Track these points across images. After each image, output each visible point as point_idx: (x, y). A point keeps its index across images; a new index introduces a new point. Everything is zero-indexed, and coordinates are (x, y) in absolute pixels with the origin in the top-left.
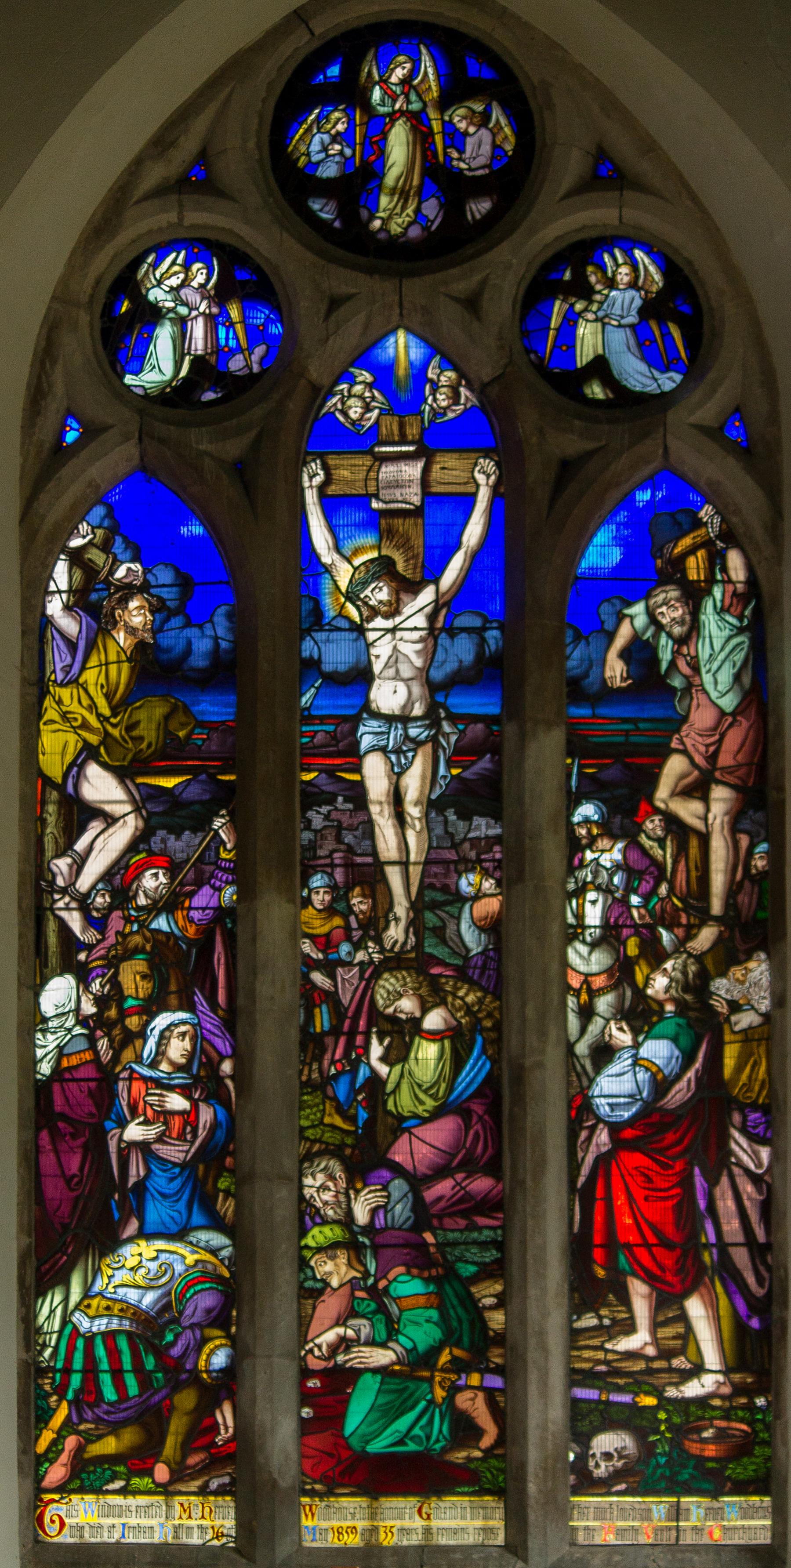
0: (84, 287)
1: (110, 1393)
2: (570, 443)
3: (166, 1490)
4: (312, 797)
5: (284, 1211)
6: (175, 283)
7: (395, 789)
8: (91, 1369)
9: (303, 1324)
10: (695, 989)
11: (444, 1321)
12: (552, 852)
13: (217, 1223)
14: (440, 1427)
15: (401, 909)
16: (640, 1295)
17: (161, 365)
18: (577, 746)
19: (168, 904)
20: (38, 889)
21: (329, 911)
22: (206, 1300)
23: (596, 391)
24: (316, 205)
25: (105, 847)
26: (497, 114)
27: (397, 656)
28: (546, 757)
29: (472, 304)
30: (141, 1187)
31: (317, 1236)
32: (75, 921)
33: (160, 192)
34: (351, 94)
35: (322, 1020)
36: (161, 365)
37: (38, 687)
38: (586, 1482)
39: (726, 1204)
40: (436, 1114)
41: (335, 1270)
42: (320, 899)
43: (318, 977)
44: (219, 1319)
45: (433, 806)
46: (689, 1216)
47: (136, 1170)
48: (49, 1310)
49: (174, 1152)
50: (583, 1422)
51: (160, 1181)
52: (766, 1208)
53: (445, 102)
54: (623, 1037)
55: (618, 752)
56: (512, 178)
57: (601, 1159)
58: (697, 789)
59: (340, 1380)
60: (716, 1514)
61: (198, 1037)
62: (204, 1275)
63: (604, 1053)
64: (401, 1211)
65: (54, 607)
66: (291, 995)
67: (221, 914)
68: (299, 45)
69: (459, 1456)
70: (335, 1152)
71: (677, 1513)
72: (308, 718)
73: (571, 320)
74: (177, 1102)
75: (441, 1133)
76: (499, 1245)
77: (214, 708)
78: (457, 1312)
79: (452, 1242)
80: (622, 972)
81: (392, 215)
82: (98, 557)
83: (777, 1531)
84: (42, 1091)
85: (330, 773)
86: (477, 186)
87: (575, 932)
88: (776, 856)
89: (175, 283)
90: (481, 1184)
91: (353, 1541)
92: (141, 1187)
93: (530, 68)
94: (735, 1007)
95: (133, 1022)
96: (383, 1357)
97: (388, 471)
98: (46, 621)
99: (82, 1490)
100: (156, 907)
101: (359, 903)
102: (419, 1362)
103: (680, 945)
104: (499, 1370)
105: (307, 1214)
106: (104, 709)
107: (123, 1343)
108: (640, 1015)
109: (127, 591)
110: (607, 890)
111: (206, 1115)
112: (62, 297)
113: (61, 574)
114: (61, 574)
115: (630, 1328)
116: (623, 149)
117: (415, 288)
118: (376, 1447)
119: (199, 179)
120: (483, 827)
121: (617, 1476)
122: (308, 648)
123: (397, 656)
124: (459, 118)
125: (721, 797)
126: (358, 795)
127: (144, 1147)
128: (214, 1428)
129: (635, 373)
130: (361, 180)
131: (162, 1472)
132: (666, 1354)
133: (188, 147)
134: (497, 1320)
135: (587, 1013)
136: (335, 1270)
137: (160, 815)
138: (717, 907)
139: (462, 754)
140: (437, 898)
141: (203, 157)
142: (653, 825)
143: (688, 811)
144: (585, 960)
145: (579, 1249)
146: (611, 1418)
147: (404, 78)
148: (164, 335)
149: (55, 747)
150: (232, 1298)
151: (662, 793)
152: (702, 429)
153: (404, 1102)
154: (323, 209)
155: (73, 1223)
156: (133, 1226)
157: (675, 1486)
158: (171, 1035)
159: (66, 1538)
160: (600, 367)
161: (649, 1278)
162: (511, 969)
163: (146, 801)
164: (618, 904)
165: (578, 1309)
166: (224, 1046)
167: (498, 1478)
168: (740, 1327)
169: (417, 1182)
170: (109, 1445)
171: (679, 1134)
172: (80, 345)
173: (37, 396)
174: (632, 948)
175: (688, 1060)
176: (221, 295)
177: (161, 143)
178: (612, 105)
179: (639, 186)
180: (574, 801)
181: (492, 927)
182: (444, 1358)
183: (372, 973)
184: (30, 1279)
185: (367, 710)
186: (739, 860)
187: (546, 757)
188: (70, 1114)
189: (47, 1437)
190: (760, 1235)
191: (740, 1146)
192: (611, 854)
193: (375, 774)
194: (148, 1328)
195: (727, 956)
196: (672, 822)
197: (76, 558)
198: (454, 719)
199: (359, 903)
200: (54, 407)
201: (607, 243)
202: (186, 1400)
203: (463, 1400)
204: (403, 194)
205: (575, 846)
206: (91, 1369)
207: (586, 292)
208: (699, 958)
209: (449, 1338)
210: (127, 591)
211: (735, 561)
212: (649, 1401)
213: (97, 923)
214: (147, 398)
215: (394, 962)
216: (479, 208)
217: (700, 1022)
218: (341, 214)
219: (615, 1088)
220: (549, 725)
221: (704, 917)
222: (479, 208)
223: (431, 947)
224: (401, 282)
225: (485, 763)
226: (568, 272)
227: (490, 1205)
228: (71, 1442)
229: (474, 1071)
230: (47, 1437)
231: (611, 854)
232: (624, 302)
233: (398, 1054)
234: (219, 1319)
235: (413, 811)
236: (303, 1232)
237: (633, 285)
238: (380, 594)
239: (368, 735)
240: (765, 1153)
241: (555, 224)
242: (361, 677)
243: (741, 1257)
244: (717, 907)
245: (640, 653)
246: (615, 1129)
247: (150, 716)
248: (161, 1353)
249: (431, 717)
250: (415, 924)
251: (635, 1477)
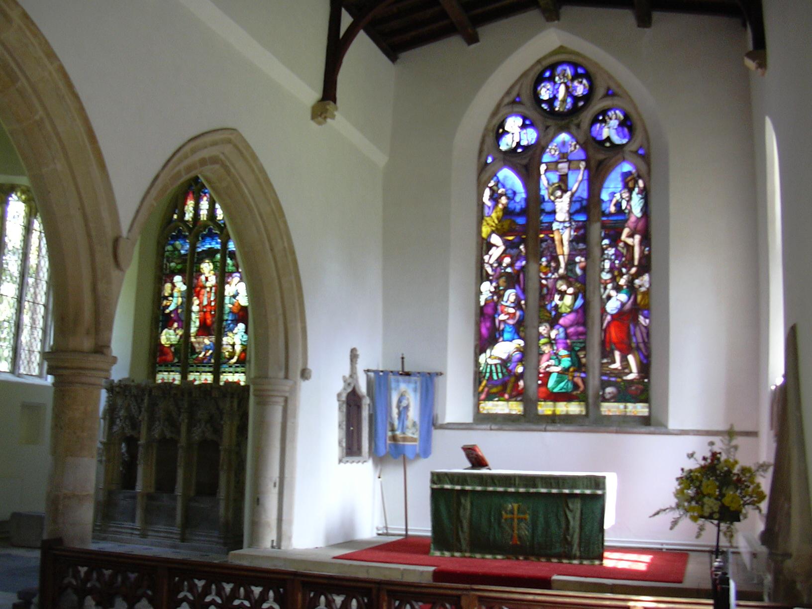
0: (491, 127)
1: (495, 377)
2: (601, 156)
3: (507, 400)
4: (543, 240)
5: (534, 335)
6: (513, 124)
8: (491, 372)
9: (539, 362)
10: (631, 283)
11: (572, 361)
13: (520, 338)
14: (570, 385)
15: (563, 265)
16: (617, 355)
18: (604, 226)
19: (511, 265)
20: (481, 263)
21: (547, 266)
22: (517, 355)
23: (519, 150)
24: (543, 106)
25: (495, 253)
28: (596, 230)
30: (503, 330)
31: (543, 341)
33: (508, 104)
35: (545, 291)
37: (481, 218)
38: (605, 400)
40: (570, 312)
41: (546, 349)
42: (544, 264)
43: (544, 282)
44: (521, 361)
45: (571, 242)
47: (502, 326)
48: (482, 359)
49: (511, 322)
50: (604, 385)
51: (508, 329)
56: (587, 98)
57: (609, 323)
58: (631, 236)
59: (548, 374)
60: (635, 407)
61: (517, 295)
62: (518, 349)
63: (609, 297)
64: (562, 335)
66: (537, 286)
67: (523, 268)
68: (539, 68)
69: (575, 393)
70: (547, 321)
71: (626, 407)
73: (601, 128)
74: (512, 311)
75: (571, 317)
76: (584, 342)
77: (521, 221)
78: (575, 359)
80: (614, 279)
82: (495, 188)
83: (650, 412)
84: (482, 308)
85: (547, 235)
87: (603, 270)
90: (581, 329)
91: (549, 413)
92: (503, 330)
94: (640, 286)
95: (502, 292)
98: (483, 203)
99: (489, 400)
100: (508, 266)
101: (553, 264)
102: (565, 371)
103: (627, 273)
104: (584, 372)
105: (540, 335)
106: (496, 221)
107: (499, 366)
108: (618, 289)
109: (501, 195)
110: (610, 260)
111: (518, 313)
112: (486, 129)
116: (614, 88)
118: (556, 390)
120: (581, 246)
121: (612, 398)
125: (637, 237)
127: (504, 321)
128: (518, 386)
129: (617, 140)
131: (506, 396)
132: (624, 368)
133: (514, 93)
134: (584, 360)
135: (605, 288)
136: (546, 349)
137: (509, 245)
138: (636, 263)
140: (571, 263)
141: (518, 96)
142: (621, 244)
143: (630, 241)
144: (606, 276)
145: (603, 344)
146: (610, 384)
149: (485, 230)
151: (623, 237)
152: (632, 152)
153: (563, 310)
155: (486, 339)
156: (501, 339)
158: (510, 295)
159: (485, 412)
161: (620, 350)
162: (587, 279)
163: (506, 242)
164: (613, 263)
165: (603, 357)
166: (522, 297)
169: (566, 328)
170: (494, 390)
172: (490, 140)
173: (481, 152)
174: (616, 273)
175: (629, 299)
177: (508, 93)
178: (611, 77)
182: (571, 369)
183: (556, 280)
184: (478, 351)
185: (555, 220)
186: (642, 252)
187: (596, 230)
189: (481, 388)
190: (646, 340)
192: (611, 251)
194: (504, 363)
195: (638, 275)
197: (491, 188)
198: (575, 221)
199: (553, 264)
200: (484, 154)
201: (609, 109)
202: (513, 379)
203: (576, 379)
206: (491, 372)
208: (632, 275)
209: (573, 365)
210: (501, 195)
212: (619, 380)
215: (561, 277)
217: (632, 289)
218: (549, 107)
219: (612, 307)
220: (596, 222)
221: (633, 266)
222: (581, 104)
223: (570, 274)
225: (582, 231)
227: (584, 334)
228: (486, 389)
229: (579, 302)
230: (481, 388)
231: (611, 251)
232: (614, 123)
233: (561, 299)
234: (521, 361)
236: (539, 340)
237: (616, 119)
240: (647, 321)
241: (597, 106)
242: (554, 212)
243: (641, 346)
244: (636, 263)
248: (507, 368)
250: (566, 269)
251: (616, 399)
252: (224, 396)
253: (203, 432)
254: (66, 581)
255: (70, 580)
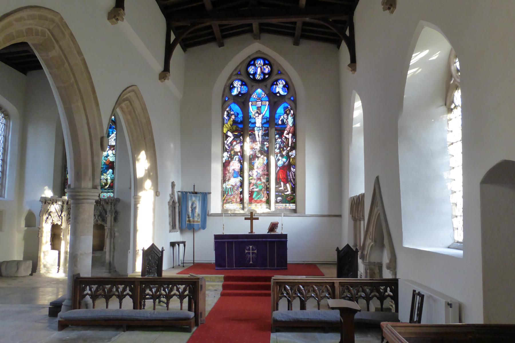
0: (228, 85)
2: (276, 100)
6: (237, 84)
10: (288, 154)
12: (274, 140)
16: (282, 183)
17: (235, 92)
18: (276, 130)
23: (278, 95)
25: (230, 140)
26: (269, 67)
27: (259, 122)
28: (273, 131)
29: (266, 86)
32: (227, 147)
34: (254, 65)
36: (235, 92)
37: (223, 124)
39: (291, 175)
46: (287, 176)
48: (224, 185)
52: (295, 175)
53: (263, 66)
54: (280, 158)
55: (280, 130)
56: (270, 74)
58: (288, 134)
65: (225, 116)
68: (249, 60)
71: (286, 205)
72: (250, 127)
77: (241, 126)
80: (280, 152)
81: (258, 77)
86: (267, 74)
87: (276, 148)
88: (296, 141)
89: (237, 84)
93: (272, 62)
96: (257, 190)
97: (258, 103)
103: (286, 149)
109: (232, 115)
113: (226, 113)
114: (226, 113)
115: (281, 187)
116: (281, 70)
117: (260, 84)
119: (239, 74)
120: (267, 138)
121: (280, 202)
122: (250, 120)
123: (259, 122)
124: (265, 67)
125: (290, 135)
126: (255, 135)
129: (282, 93)
130: (255, 74)
132: (285, 189)
133: (238, 70)
139: (265, 131)
141: (240, 71)
142: (284, 137)
143: (287, 136)
147: (260, 62)
148: (236, 89)
149: (225, 130)
151: (285, 134)
154: (251, 77)
157: (286, 203)
160: (279, 92)
163: (234, 135)
168: (292, 187)
172: (227, 90)
176: (241, 85)
177: (235, 70)
179: (283, 74)
180: (276, 135)
181: (268, 147)
186: (292, 141)
191: (292, 169)
193: (256, 133)
195: (291, 150)
196: (285, 137)
197: (227, 111)
200: (225, 96)
204: (259, 75)
205: (276, 140)
207: (277, 85)
210: (232, 115)
211: (292, 112)
213: (229, 147)
214: (234, 96)
216: (267, 76)
217: (288, 157)
221: (289, 146)
224: (252, 231)
226: (275, 83)
231: (279, 140)
232: (281, 86)
235: (260, 136)
238: (257, 115)
239: (256, 129)
242: (255, 123)
243: (292, 180)
245: (282, 121)
246: (280, 167)
247: (234, 127)
249: (262, 127)
252: (107, 203)
253: (97, 221)
254: (85, 292)
255: (88, 291)
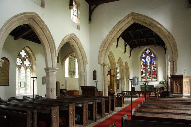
6: (143, 55)
7: (148, 65)
25: (142, 66)
79: (150, 74)
89: (143, 55)
140: (149, 67)
147: (148, 50)
150: (145, 75)
155: (142, 74)
158: (144, 70)
167: (151, 79)
171: (154, 72)
188: (142, 72)
217: (155, 70)
219: (153, 71)
